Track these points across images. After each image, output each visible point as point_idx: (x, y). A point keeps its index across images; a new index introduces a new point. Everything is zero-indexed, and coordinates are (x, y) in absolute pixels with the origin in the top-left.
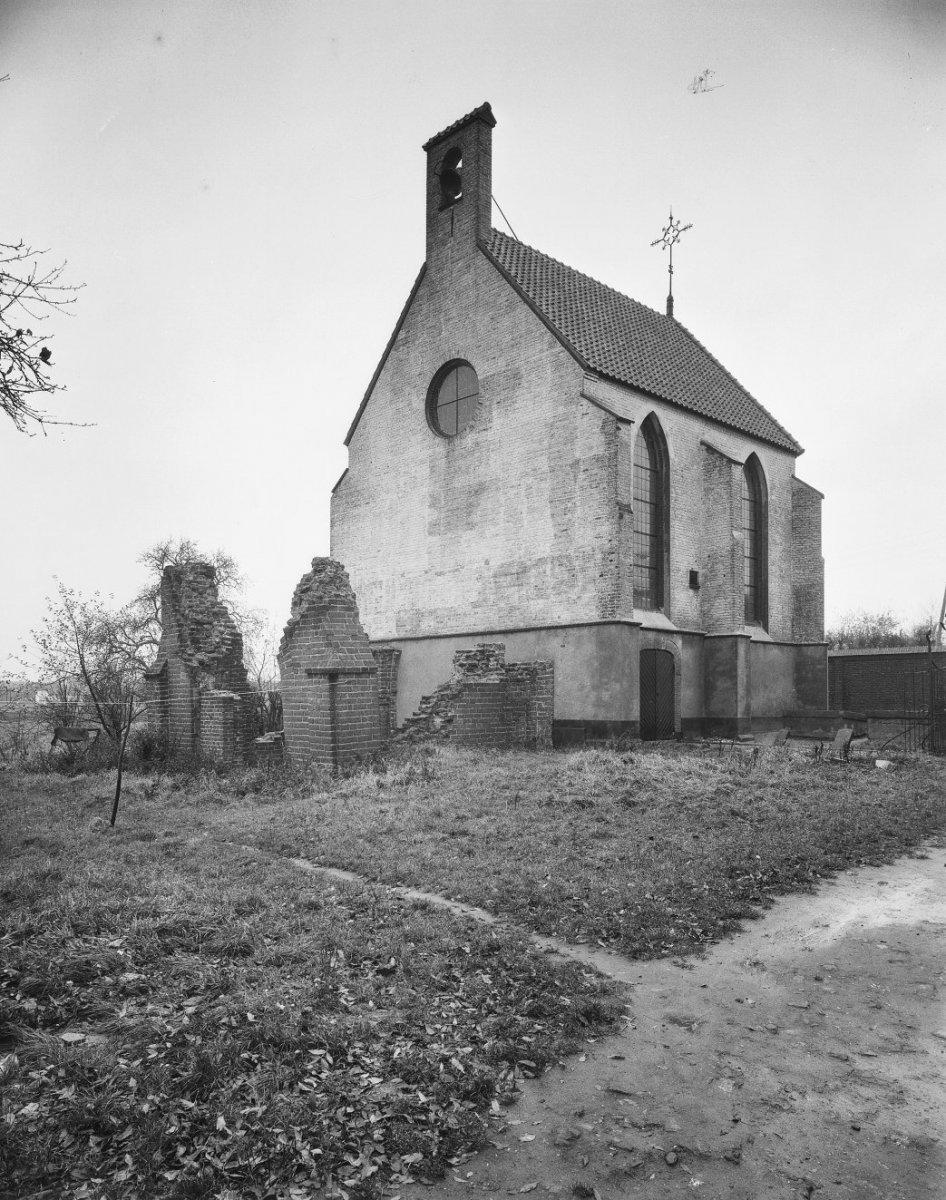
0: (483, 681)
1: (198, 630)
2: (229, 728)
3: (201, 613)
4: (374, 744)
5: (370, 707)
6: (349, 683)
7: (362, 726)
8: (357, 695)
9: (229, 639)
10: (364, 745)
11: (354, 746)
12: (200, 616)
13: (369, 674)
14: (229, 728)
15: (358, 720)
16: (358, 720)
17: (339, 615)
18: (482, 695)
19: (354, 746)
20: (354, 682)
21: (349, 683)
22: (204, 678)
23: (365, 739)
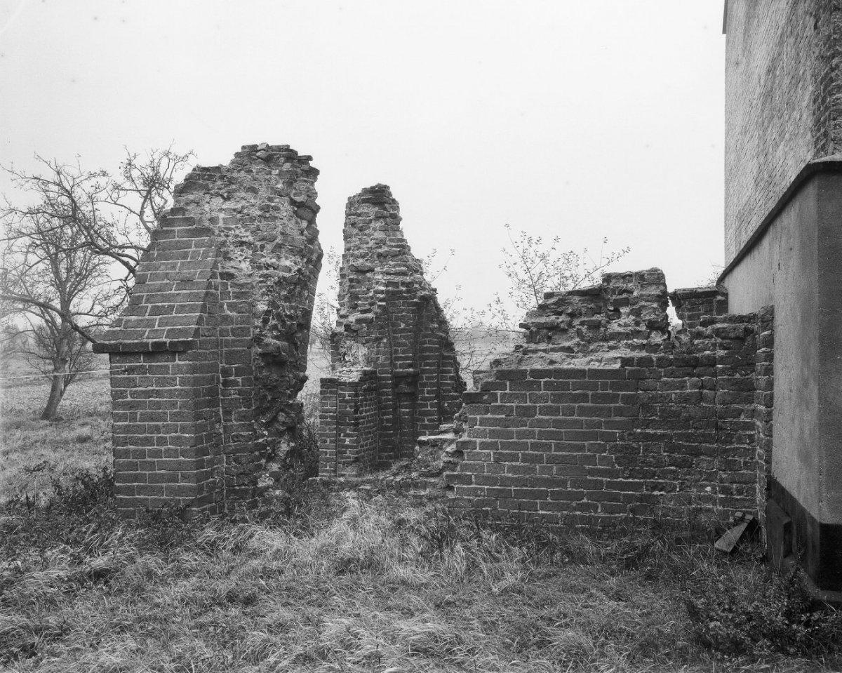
0: (579, 363)
1: (358, 282)
2: (328, 424)
3: (363, 256)
4: (181, 491)
5: (176, 417)
6: (130, 370)
7: (157, 454)
8: (148, 394)
9: (382, 292)
10: (160, 490)
11: (140, 490)
12: (361, 261)
13: (174, 353)
14: (328, 424)
15: (148, 441)
16: (148, 441)
17: (178, 246)
18: (558, 398)
19: (140, 490)
20: (142, 370)
21: (130, 370)
22: (350, 348)
23: (162, 478)
